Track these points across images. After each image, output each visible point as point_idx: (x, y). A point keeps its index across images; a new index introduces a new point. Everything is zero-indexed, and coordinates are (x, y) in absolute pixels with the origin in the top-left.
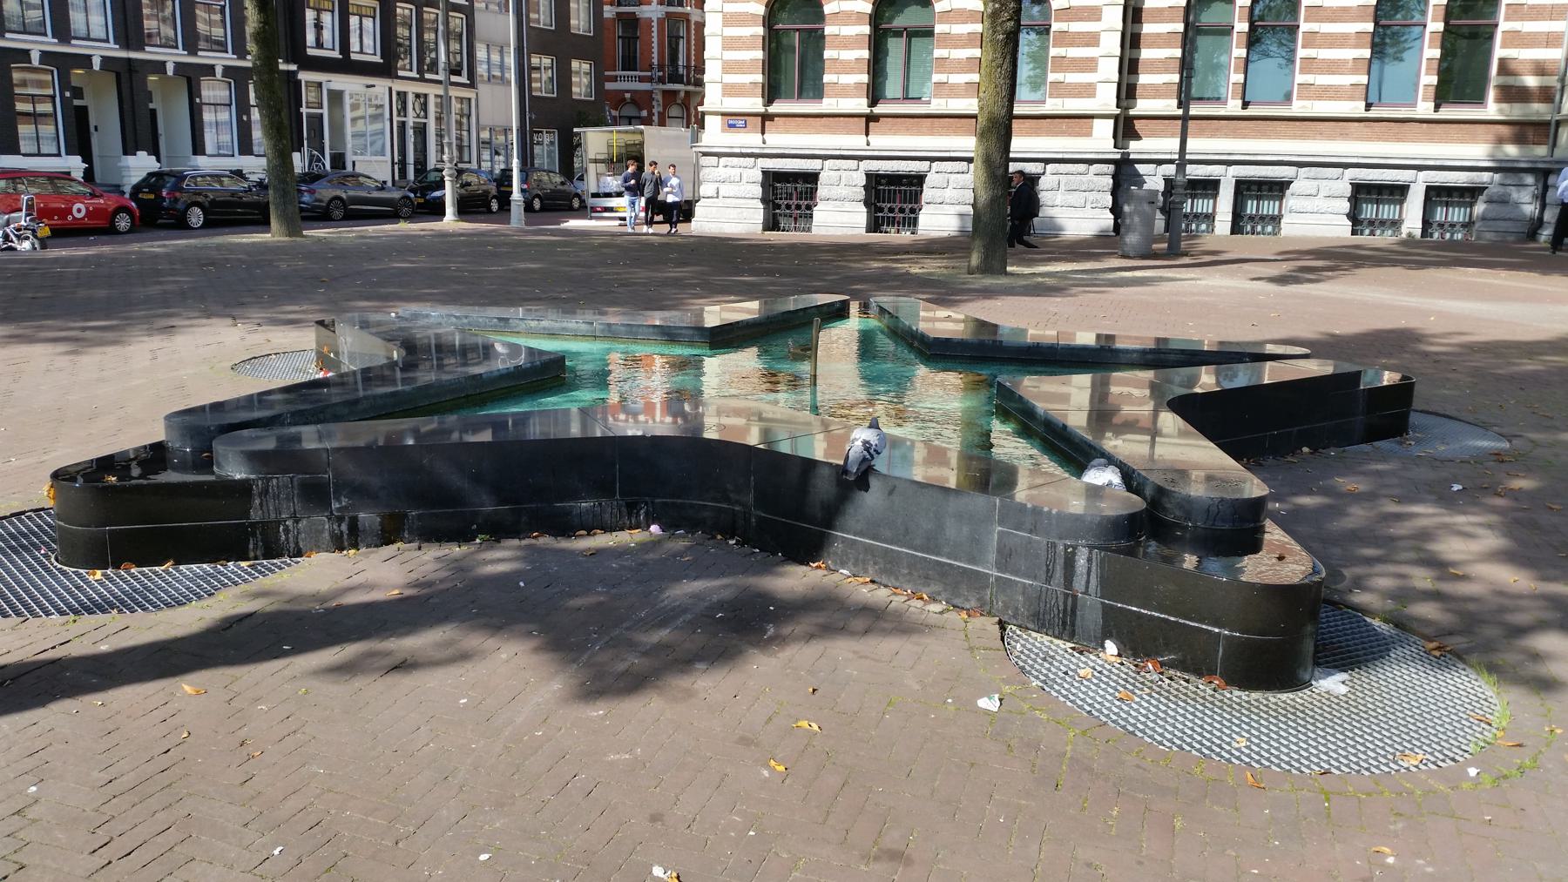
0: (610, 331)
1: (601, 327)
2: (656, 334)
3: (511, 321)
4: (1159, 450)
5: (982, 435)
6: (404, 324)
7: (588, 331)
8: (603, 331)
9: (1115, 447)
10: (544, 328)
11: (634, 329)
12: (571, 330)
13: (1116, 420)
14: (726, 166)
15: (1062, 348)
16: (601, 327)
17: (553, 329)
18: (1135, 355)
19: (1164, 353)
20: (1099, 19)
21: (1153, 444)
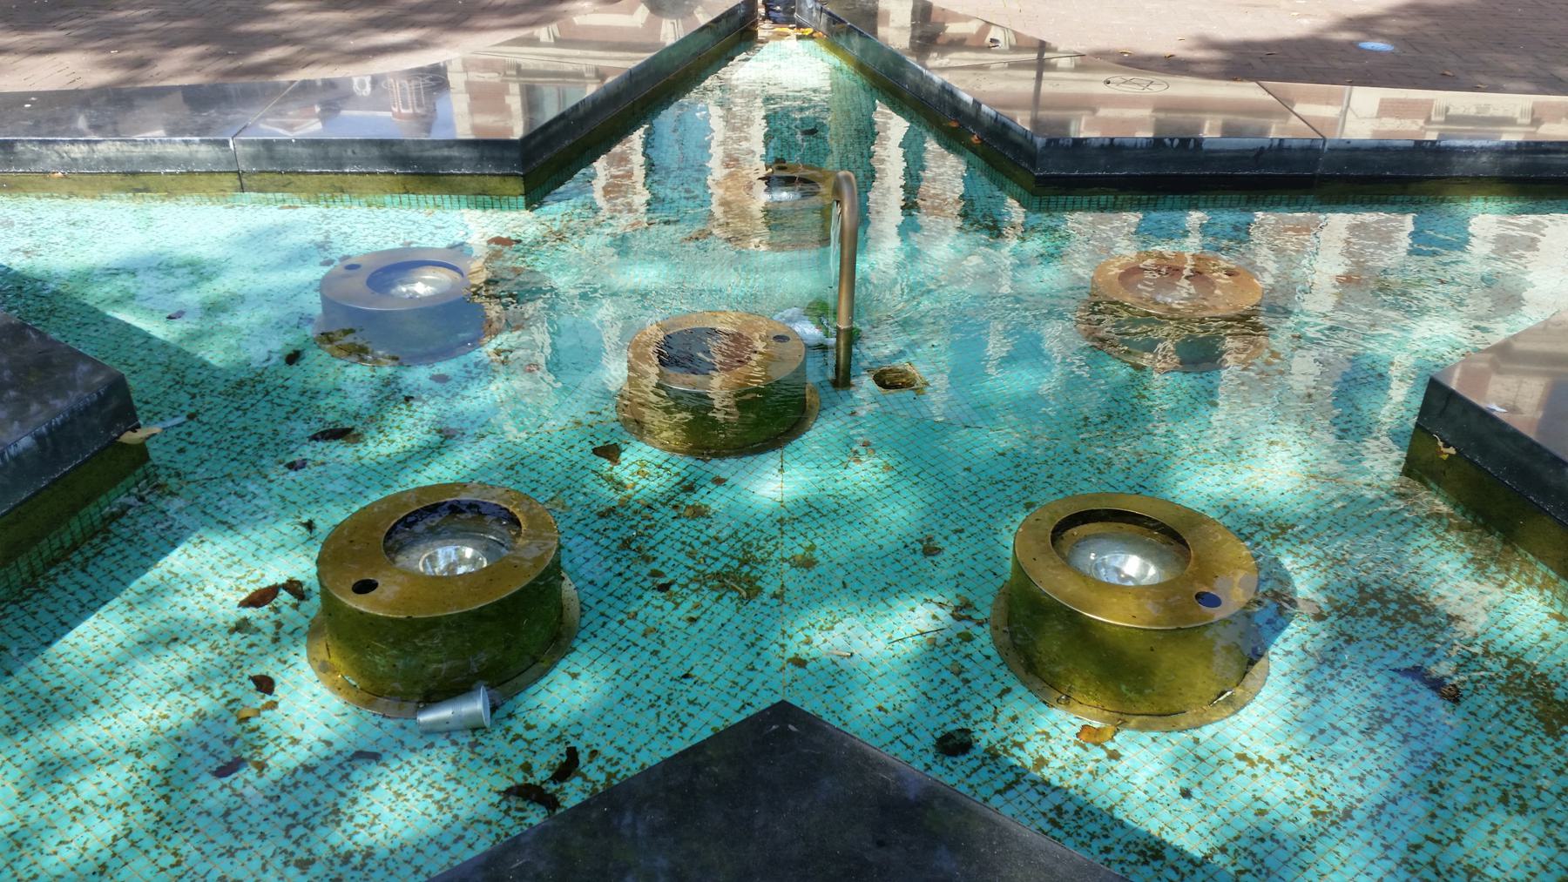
0: (272, 158)
1: (248, 149)
2: (369, 161)
3: (19, 147)
4: (1046, 87)
5: (917, 229)
6: (1044, 219)
7: (217, 162)
8: (255, 159)
9: (263, 698)
10: (108, 161)
11: (333, 151)
12: (176, 162)
13: (939, 41)
14: (45, 681)
15: (1331, 150)
16: (248, 149)
17: (130, 160)
18: (1484, 159)
19: (1547, 151)
20: (1382, 101)
21: (1039, 78)
